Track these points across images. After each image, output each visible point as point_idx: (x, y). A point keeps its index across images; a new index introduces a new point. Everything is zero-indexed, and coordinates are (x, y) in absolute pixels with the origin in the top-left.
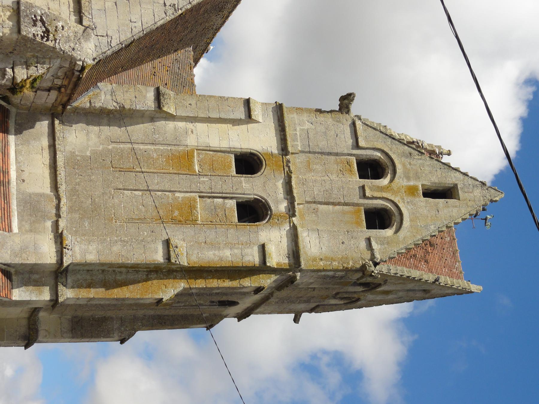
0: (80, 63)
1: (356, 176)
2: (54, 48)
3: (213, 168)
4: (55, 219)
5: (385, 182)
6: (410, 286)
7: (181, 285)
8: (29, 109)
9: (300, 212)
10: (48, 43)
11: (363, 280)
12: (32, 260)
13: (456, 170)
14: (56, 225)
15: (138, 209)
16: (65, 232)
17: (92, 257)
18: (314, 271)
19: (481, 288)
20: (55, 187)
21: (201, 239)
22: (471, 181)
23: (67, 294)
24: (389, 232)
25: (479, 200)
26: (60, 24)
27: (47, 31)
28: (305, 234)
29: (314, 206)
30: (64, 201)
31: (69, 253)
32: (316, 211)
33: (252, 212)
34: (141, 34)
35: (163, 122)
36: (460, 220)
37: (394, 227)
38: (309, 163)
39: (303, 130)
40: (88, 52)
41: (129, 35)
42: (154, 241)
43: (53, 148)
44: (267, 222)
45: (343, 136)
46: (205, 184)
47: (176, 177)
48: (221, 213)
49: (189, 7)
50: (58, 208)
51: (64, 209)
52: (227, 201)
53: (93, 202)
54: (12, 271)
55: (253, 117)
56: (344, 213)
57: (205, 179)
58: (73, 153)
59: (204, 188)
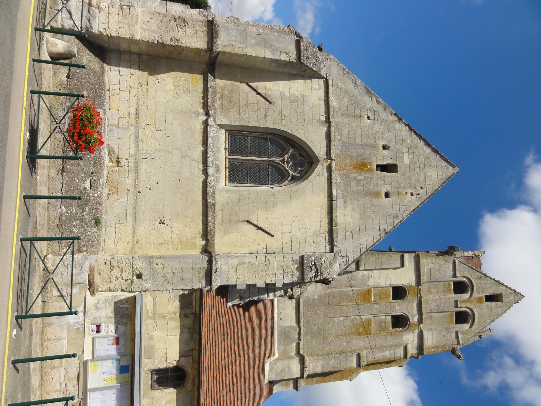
4: (297, 341)
13: (502, 284)
22: (509, 291)
30: (302, 329)
33: (400, 322)
37: (470, 323)
38: (429, 288)
39: (428, 268)
44: (407, 329)
45: (448, 270)
48: (383, 325)
50: (299, 334)
51: (302, 333)
53: (318, 327)
56: (445, 317)
58: (308, 298)
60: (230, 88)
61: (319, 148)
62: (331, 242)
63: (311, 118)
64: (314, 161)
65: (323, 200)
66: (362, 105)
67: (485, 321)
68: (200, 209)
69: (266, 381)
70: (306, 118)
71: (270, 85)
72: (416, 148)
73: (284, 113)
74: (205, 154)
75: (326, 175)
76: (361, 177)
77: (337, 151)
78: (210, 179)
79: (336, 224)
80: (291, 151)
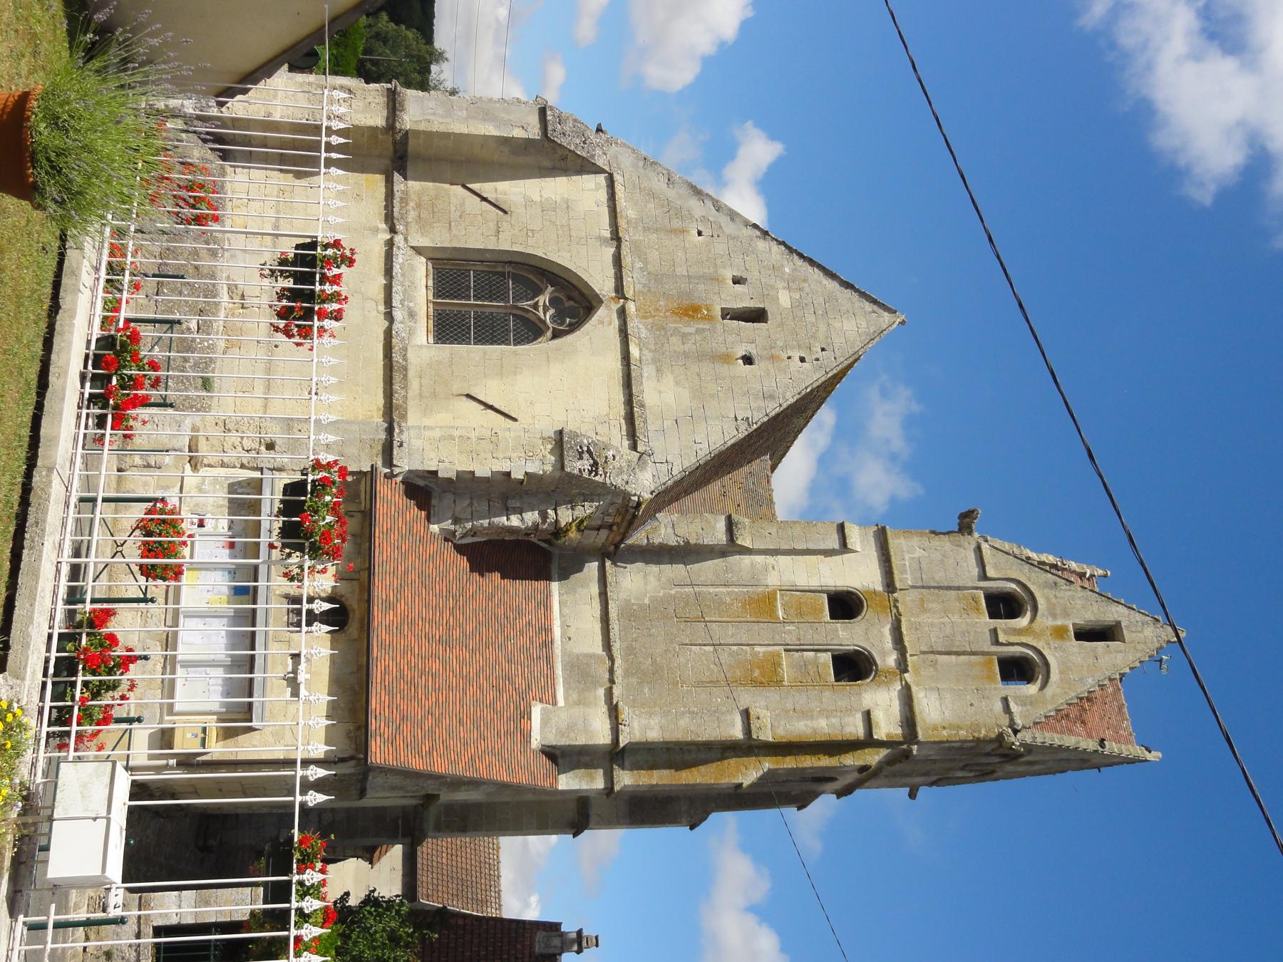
0: (635, 498)
1: (985, 617)
2: (605, 484)
3: (800, 612)
4: (608, 685)
5: (1023, 622)
6: (1064, 755)
7: (768, 764)
8: (575, 549)
9: (914, 666)
10: (597, 478)
11: (1001, 751)
12: (581, 740)
14: (609, 693)
15: (709, 669)
16: (621, 704)
17: (654, 735)
18: (935, 742)
19: (1160, 755)
20: (607, 645)
21: (789, 706)
23: (625, 779)
24: (1032, 689)
25: (1152, 642)
26: (610, 453)
27: (595, 464)
28: (921, 695)
29: (931, 657)
30: (618, 662)
31: (626, 729)
32: (934, 664)
33: (852, 667)
34: (708, 458)
35: (737, 557)
36: (1127, 670)
37: (1039, 681)
40: (644, 484)
41: (694, 460)
42: (730, 712)
43: (604, 596)
46: (791, 633)
47: (755, 627)
48: (812, 670)
49: (766, 419)
50: (611, 671)
51: (619, 672)
52: (819, 654)
53: (654, 662)
54: (558, 753)
55: (849, 546)
56: (971, 665)
57: (791, 628)
58: (627, 601)
59: (789, 639)
60: (432, 193)
61: (600, 280)
62: (632, 435)
63: (583, 234)
64: (594, 304)
65: (616, 365)
66: (685, 213)
67: (1081, 680)
68: (381, 372)
69: (536, 741)
70: (573, 233)
71: (503, 186)
72: (805, 281)
73: (530, 227)
74: (388, 290)
75: (616, 323)
76: (692, 330)
77: (638, 287)
78: (396, 326)
79: (642, 406)
80: (550, 289)
